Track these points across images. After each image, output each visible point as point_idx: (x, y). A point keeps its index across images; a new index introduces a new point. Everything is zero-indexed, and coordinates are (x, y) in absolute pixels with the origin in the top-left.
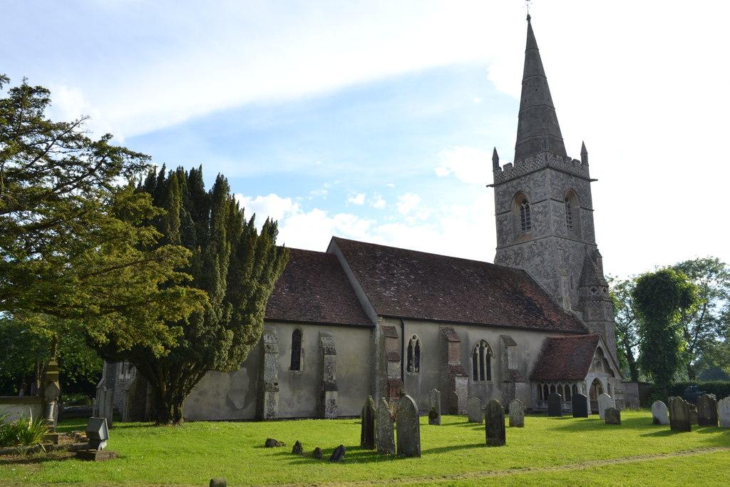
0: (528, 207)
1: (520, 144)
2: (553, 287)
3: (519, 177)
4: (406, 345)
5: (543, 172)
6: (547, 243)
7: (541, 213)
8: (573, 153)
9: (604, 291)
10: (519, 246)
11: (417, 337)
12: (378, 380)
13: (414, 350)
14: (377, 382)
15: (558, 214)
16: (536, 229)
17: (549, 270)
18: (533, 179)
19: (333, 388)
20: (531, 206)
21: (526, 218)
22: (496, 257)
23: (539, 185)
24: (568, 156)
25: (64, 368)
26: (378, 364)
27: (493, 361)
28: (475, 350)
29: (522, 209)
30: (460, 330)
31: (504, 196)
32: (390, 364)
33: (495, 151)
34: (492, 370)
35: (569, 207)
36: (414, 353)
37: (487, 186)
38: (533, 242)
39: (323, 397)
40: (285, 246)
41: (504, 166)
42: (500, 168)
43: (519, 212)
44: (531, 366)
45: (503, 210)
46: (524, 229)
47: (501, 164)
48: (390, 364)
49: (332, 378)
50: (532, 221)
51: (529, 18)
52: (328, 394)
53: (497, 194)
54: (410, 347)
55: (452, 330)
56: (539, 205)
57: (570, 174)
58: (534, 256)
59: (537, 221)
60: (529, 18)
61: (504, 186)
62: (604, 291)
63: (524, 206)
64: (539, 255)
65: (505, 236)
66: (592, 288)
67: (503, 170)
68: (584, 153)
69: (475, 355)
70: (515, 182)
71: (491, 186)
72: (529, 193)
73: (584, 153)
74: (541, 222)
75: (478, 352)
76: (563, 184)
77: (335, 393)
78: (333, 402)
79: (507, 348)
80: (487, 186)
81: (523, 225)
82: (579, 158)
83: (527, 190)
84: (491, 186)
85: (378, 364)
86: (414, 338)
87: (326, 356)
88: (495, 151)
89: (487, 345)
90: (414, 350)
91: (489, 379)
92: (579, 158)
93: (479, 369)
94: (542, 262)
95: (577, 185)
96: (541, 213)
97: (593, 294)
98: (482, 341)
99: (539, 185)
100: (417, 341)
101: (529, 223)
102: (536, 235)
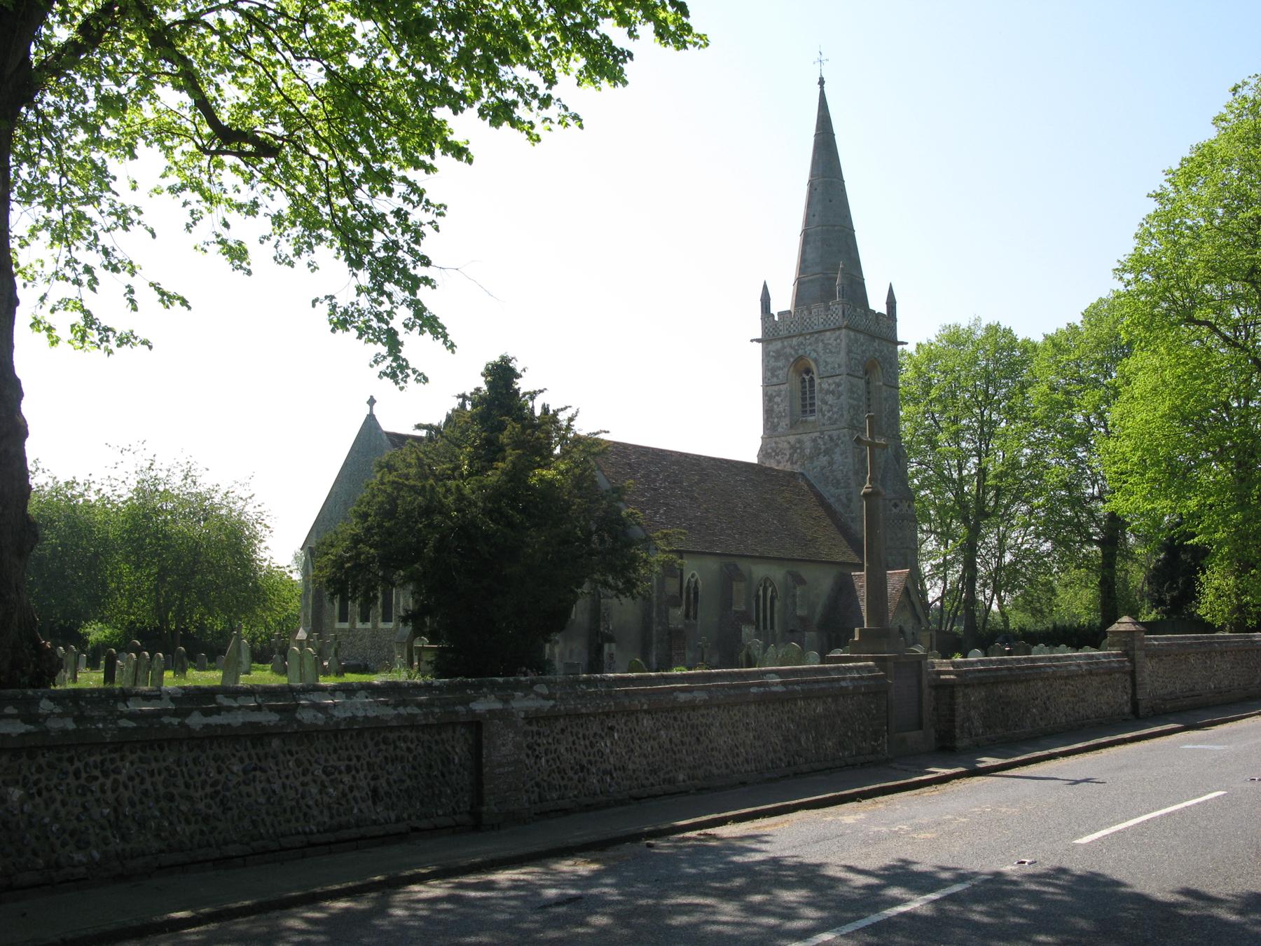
0: (812, 380)
1: (804, 283)
2: (845, 500)
3: (801, 335)
4: (685, 584)
5: (837, 333)
6: (839, 438)
7: (832, 392)
8: (877, 303)
9: (909, 506)
10: (798, 436)
11: (697, 575)
12: (656, 628)
13: (692, 591)
14: (654, 632)
15: (855, 396)
16: (824, 415)
17: (839, 476)
18: (822, 341)
19: (610, 639)
20: (817, 381)
21: (808, 401)
22: (761, 450)
23: (831, 352)
24: (871, 307)
25: (1039, 507)
26: (655, 610)
27: (777, 604)
28: (758, 590)
29: (804, 380)
30: (743, 565)
31: (777, 358)
32: (671, 610)
33: (765, 287)
34: (776, 616)
35: (868, 383)
36: (692, 595)
37: (752, 341)
38: (817, 434)
39: (600, 649)
40: (760, 336)
41: (780, 314)
42: (773, 315)
43: (799, 385)
44: (819, 609)
45: (775, 380)
46: (804, 412)
47: (775, 309)
48: (671, 610)
49: (608, 628)
50: (818, 403)
51: (822, 82)
52: (606, 646)
53: (766, 354)
54: (688, 587)
55: (736, 566)
56: (830, 381)
57: (873, 337)
58: (819, 454)
59: (826, 403)
60: (822, 82)
61: (778, 345)
62: (909, 506)
63: (807, 378)
64: (827, 452)
65: (776, 420)
66: (893, 502)
67: (776, 319)
68: (891, 302)
69: (758, 597)
70: (795, 341)
71: (758, 340)
72: (816, 361)
73: (891, 302)
74: (831, 406)
75: (761, 593)
76: (864, 352)
77: (613, 645)
78: (611, 656)
79: (795, 588)
80: (752, 341)
81: (804, 406)
82: (884, 311)
83: (814, 355)
84: (758, 340)
85: (655, 610)
86: (693, 576)
87: (602, 601)
88: (765, 287)
89: (772, 584)
90: (692, 591)
91: (772, 628)
92: (884, 311)
93: (761, 615)
94: (831, 463)
95: (881, 352)
96: (832, 392)
97: (894, 510)
98: (767, 579)
99: (831, 352)
100: (696, 582)
101: (812, 405)
102: (824, 425)
